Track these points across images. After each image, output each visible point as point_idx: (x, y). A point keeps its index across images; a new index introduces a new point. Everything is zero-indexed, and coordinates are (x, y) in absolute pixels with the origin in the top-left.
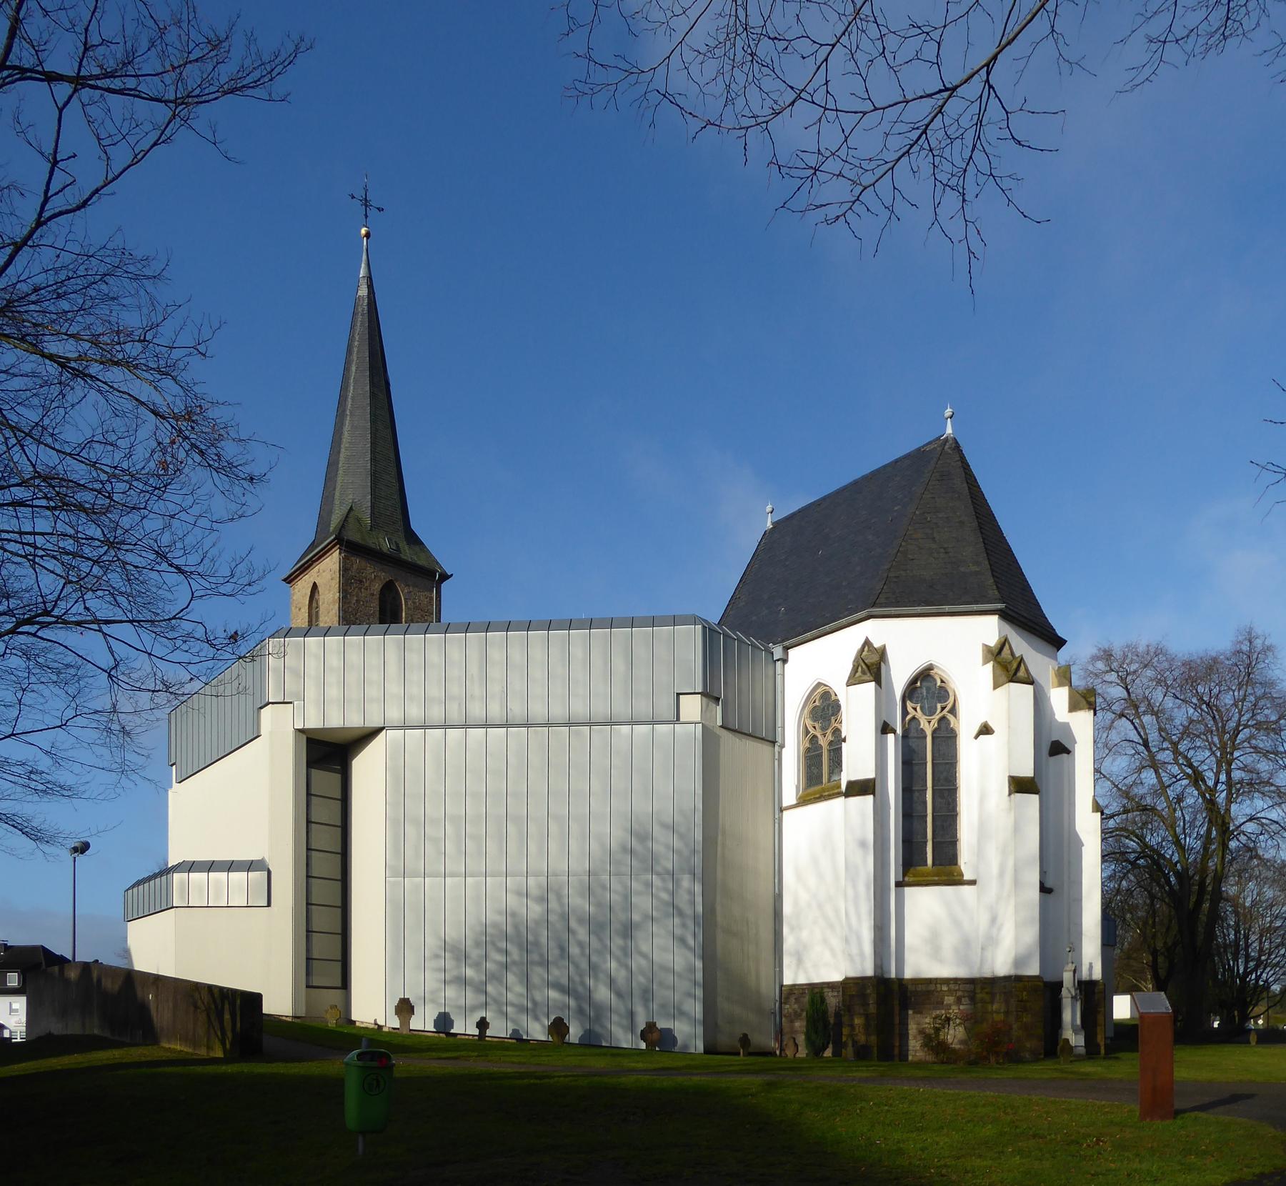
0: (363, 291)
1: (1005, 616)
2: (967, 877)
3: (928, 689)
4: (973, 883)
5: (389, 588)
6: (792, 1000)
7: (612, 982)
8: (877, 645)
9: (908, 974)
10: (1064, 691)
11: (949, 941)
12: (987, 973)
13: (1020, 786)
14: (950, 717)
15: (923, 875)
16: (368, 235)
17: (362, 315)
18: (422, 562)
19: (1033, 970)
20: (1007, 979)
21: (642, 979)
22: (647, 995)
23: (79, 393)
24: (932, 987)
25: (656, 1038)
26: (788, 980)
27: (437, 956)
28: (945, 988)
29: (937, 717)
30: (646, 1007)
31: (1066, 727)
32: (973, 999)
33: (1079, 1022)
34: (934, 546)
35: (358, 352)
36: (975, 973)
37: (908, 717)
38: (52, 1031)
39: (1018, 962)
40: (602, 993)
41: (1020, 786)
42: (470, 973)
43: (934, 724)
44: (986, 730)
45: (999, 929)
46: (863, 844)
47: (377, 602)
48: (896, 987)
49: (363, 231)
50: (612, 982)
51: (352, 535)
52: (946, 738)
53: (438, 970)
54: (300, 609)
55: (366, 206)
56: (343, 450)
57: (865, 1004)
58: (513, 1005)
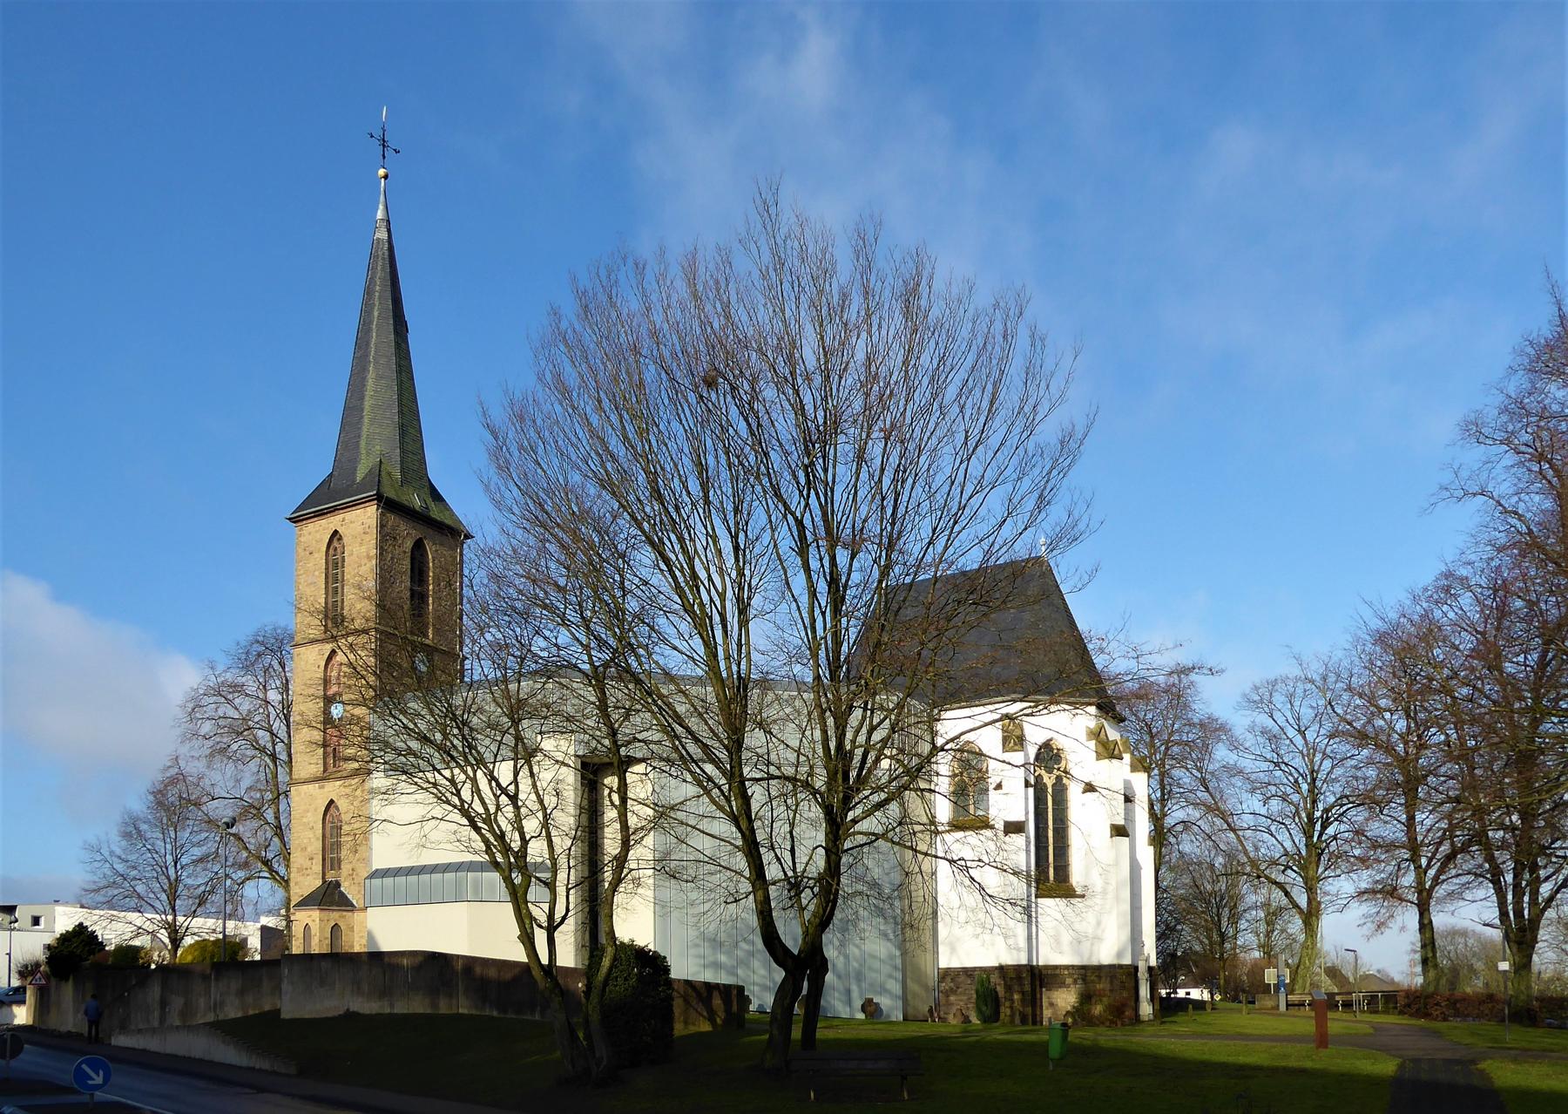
0: (382, 234)
2: (1079, 891)
4: (1083, 896)
5: (419, 546)
6: (949, 979)
12: (1095, 962)
16: (386, 177)
17: (383, 259)
18: (448, 522)
19: (1127, 961)
20: (1112, 968)
21: (855, 964)
22: (859, 977)
23: (1481, 893)
24: (1058, 972)
25: (870, 1008)
26: (943, 964)
27: (697, 946)
28: (1066, 972)
30: (859, 987)
32: (1084, 979)
36: (1085, 962)
39: (1120, 954)
42: (723, 958)
45: (1103, 931)
47: (409, 560)
48: (1037, 972)
49: (382, 172)
51: (389, 493)
52: (1060, 791)
53: (699, 956)
55: (384, 146)
56: (367, 398)
57: (1021, 985)
58: (758, 985)
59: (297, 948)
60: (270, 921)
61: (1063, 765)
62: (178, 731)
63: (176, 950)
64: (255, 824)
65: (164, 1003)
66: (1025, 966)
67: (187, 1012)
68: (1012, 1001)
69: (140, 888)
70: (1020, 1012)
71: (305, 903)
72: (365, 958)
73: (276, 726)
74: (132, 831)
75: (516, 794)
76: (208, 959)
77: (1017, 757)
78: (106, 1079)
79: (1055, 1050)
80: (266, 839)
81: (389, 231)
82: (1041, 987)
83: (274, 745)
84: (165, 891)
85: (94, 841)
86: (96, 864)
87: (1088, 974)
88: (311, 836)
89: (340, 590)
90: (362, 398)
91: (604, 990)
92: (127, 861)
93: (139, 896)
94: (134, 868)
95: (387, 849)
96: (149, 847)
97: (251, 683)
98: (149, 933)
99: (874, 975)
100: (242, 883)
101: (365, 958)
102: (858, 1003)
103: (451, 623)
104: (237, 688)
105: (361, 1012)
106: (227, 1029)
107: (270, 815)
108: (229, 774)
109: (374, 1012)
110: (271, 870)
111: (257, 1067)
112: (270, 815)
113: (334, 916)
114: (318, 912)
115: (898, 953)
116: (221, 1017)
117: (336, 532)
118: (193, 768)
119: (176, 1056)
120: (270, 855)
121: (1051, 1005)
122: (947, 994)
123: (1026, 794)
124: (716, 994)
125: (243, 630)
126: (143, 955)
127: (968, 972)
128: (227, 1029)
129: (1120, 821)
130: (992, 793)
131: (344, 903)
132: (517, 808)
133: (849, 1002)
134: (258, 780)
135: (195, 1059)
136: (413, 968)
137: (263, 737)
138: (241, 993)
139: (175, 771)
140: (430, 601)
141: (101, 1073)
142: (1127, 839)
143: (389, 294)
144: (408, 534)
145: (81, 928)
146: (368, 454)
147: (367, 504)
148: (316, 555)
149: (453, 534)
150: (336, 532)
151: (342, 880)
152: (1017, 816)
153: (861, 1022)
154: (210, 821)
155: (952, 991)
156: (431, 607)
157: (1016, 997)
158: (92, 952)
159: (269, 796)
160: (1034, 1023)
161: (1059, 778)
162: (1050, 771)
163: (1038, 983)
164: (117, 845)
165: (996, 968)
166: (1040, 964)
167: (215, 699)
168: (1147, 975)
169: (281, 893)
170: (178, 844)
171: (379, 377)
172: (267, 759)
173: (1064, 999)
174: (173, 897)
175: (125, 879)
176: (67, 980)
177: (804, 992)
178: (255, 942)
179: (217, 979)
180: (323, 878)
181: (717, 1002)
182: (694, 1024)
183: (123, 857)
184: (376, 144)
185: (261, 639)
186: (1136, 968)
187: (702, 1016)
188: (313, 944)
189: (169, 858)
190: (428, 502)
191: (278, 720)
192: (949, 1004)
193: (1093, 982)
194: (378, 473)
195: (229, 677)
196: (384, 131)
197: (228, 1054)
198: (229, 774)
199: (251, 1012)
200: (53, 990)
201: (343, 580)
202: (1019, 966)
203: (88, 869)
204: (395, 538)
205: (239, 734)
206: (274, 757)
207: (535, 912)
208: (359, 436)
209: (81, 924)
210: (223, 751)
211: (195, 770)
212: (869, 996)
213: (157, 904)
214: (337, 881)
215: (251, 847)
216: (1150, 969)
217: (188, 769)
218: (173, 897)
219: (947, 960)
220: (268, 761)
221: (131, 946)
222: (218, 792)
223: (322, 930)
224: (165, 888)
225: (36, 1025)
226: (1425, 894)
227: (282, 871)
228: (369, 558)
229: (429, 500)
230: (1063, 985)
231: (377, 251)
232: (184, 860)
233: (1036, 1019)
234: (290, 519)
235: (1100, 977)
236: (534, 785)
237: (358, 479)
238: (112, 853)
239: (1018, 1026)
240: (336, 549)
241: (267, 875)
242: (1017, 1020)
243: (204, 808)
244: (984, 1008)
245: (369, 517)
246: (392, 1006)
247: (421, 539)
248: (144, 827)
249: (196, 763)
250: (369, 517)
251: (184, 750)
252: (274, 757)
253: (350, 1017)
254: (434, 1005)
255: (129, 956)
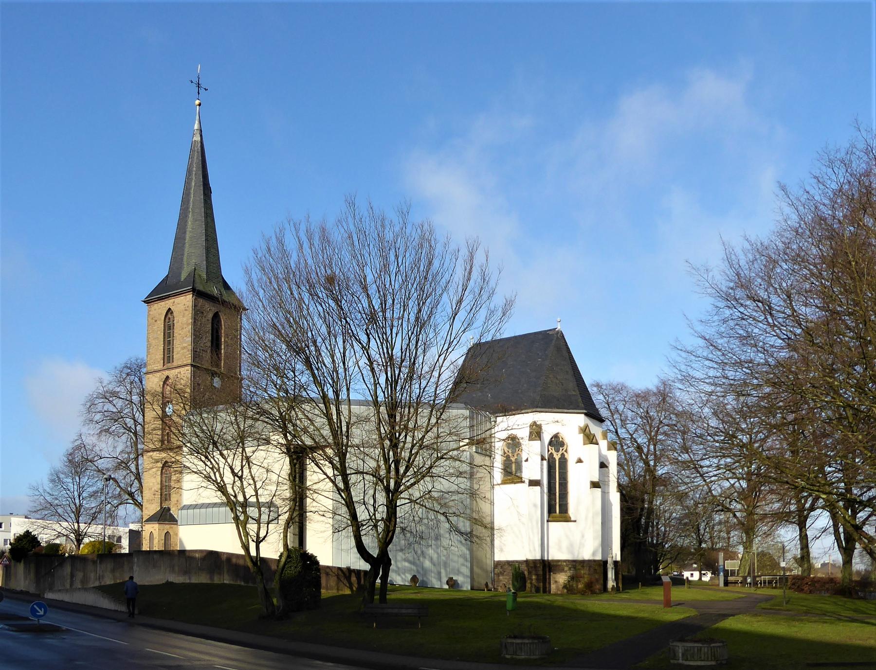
0: (197, 138)
1: (586, 414)
2: (572, 519)
3: (557, 441)
5: (216, 316)
7: (431, 560)
8: (538, 423)
9: (550, 558)
10: (606, 441)
11: (565, 544)
12: (580, 558)
13: (595, 485)
14: (565, 453)
15: (555, 518)
16: (200, 105)
19: (599, 557)
20: (589, 561)
22: (446, 565)
24: (560, 563)
25: (452, 583)
26: (496, 559)
28: (565, 564)
29: (560, 453)
30: (446, 570)
31: (606, 456)
33: (614, 578)
34: (558, 382)
35: (195, 174)
36: (575, 558)
37: (550, 452)
38: (169, 580)
39: (594, 554)
40: (427, 564)
41: (595, 485)
43: (559, 456)
44: (580, 461)
46: (535, 506)
48: (547, 563)
49: (197, 102)
50: (431, 560)
51: (199, 287)
52: (563, 461)
54: (156, 321)
55: (199, 87)
56: (188, 233)
59: (145, 547)
60: (134, 527)
61: (565, 448)
62: (82, 419)
63: (79, 544)
64: (125, 473)
65: (72, 576)
66: (539, 560)
67: (84, 581)
68: (532, 580)
69: (60, 510)
70: (535, 586)
71: (151, 519)
72: (176, 553)
73: (137, 415)
74: (56, 479)
75: (242, 475)
76: (96, 551)
77: (537, 444)
78: (45, 612)
79: (509, 606)
80: (131, 481)
81: (201, 136)
82: (550, 572)
83: (136, 426)
84: (73, 512)
85: (35, 484)
86: (36, 497)
87: (576, 565)
88: (155, 481)
89: (171, 342)
90: (185, 233)
91: (282, 573)
92: (53, 495)
93: (60, 515)
94: (57, 499)
95: (188, 498)
96: (65, 487)
97: (123, 391)
98: (64, 535)
99: (454, 564)
100: (117, 506)
101: (176, 553)
102: (445, 580)
103: (235, 358)
104: (115, 394)
105: (174, 582)
106: (104, 590)
107: (133, 467)
108: (110, 442)
109: (181, 582)
110: (133, 499)
111: (119, 610)
112: (133, 467)
113: (167, 527)
114: (157, 525)
115: (468, 552)
116: (102, 584)
117: (170, 309)
118: (90, 440)
119: (78, 604)
120: (133, 490)
121: (556, 582)
122: (498, 575)
123: (542, 465)
124: (353, 575)
125: (120, 360)
126: (61, 549)
127: (509, 563)
128: (104, 590)
129: (596, 479)
130: (524, 464)
131: (173, 520)
132: (242, 482)
133: (440, 579)
134: (127, 447)
135: (88, 606)
136: (201, 559)
137: (130, 422)
138: (113, 571)
139: (79, 442)
140: (223, 347)
141: (43, 609)
142: (600, 489)
143: (200, 172)
144: (210, 309)
145: (28, 533)
146: (188, 264)
147: (187, 294)
148: (158, 322)
149: (237, 308)
150: (170, 309)
151: (171, 507)
152: (538, 477)
153: (446, 590)
154: (99, 471)
155: (502, 574)
156: (223, 351)
157: (534, 577)
158: (34, 547)
159: (132, 456)
160: (545, 591)
161: (563, 455)
162: (557, 451)
163: (547, 569)
164: (48, 486)
165: (525, 561)
166: (550, 559)
167: (102, 400)
168: (612, 566)
169: (138, 512)
170: (81, 486)
171: (195, 220)
172: (131, 434)
173: (561, 578)
174: (78, 514)
175: (51, 505)
176: (20, 562)
177: (381, 573)
178: (125, 543)
179: (100, 563)
180: (161, 505)
181: (354, 579)
182: (342, 590)
183: (51, 492)
184: (194, 86)
185: (129, 365)
186: (605, 563)
187: (346, 585)
188: (155, 543)
189: (76, 494)
190: (222, 291)
191: (138, 413)
192: (499, 581)
193: (579, 569)
194: (194, 274)
195: (111, 387)
196: (199, 78)
197: (105, 603)
198: (110, 442)
199: (118, 581)
200: (12, 568)
201: (173, 337)
202: (536, 560)
203: (31, 499)
204: (203, 313)
205: (116, 421)
206: (135, 434)
207: (251, 533)
208: (183, 255)
209: (28, 531)
210: (107, 431)
211: (91, 442)
212: (451, 576)
213: (69, 519)
214: (168, 507)
215: (122, 485)
216: (616, 563)
217: (87, 441)
218: (78, 514)
219: (499, 557)
220: (133, 436)
221: (55, 544)
222: (104, 454)
223: (159, 535)
224: (74, 510)
225: (4, 586)
226: (802, 518)
227: (139, 499)
228: (188, 325)
229: (223, 290)
230: (563, 570)
231: (194, 148)
232: (85, 495)
233: (546, 590)
234: (144, 302)
235: (583, 566)
236: (250, 472)
237: (182, 279)
238: (45, 491)
239: (533, 593)
240: (169, 319)
241: (131, 501)
242: (533, 590)
243: (95, 463)
244: (516, 583)
245: (188, 301)
246: (190, 579)
247: (217, 312)
248: (62, 476)
249: (91, 438)
250: (188, 301)
251: (84, 430)
252: (135, 434)
253: (169, 584)
254: (212, 578)
255: (54, 548)
